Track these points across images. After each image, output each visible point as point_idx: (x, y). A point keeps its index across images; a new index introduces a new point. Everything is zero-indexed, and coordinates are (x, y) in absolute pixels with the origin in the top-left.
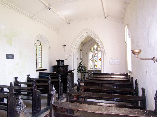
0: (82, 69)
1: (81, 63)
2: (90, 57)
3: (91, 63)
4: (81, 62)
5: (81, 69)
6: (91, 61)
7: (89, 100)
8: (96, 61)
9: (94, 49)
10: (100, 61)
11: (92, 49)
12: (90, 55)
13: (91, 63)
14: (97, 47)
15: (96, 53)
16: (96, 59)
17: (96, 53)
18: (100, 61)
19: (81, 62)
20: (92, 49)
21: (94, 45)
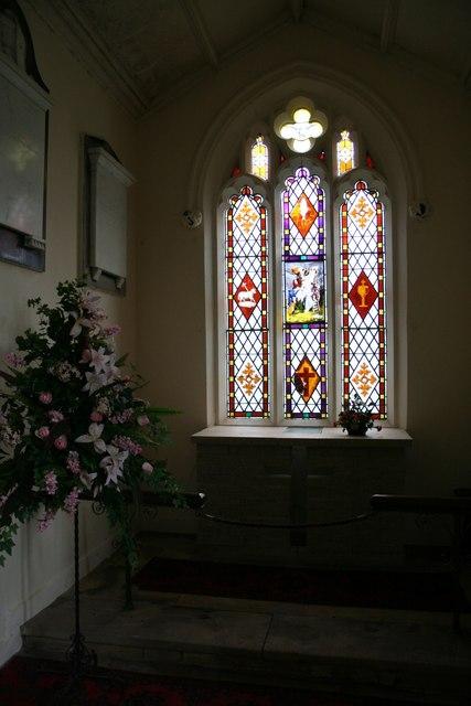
0: (90, 456)
1: (58, 326)
2: (223, 266)
3: (248, 349)
4: (55, 316)
5: (59, 458)
6: (248, 313)
7: (14, 376)
8: (306, 316)
9: (282, 156)
10: (363, 313)
11: (259, 160)
12: (223, 235)
13: (248, 349)
14: (317, 130)
15: (362, 291)
16: (305, 293)
17: (362, 291)
18: (363, 313)
19: (55, 316)
20: (259, 160)
21: (284, 113)
